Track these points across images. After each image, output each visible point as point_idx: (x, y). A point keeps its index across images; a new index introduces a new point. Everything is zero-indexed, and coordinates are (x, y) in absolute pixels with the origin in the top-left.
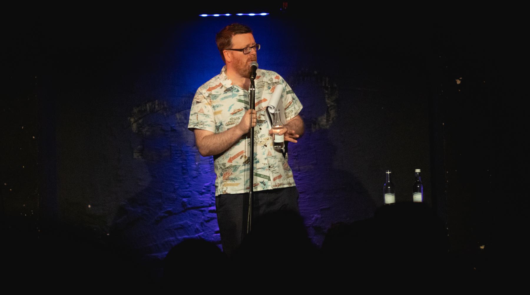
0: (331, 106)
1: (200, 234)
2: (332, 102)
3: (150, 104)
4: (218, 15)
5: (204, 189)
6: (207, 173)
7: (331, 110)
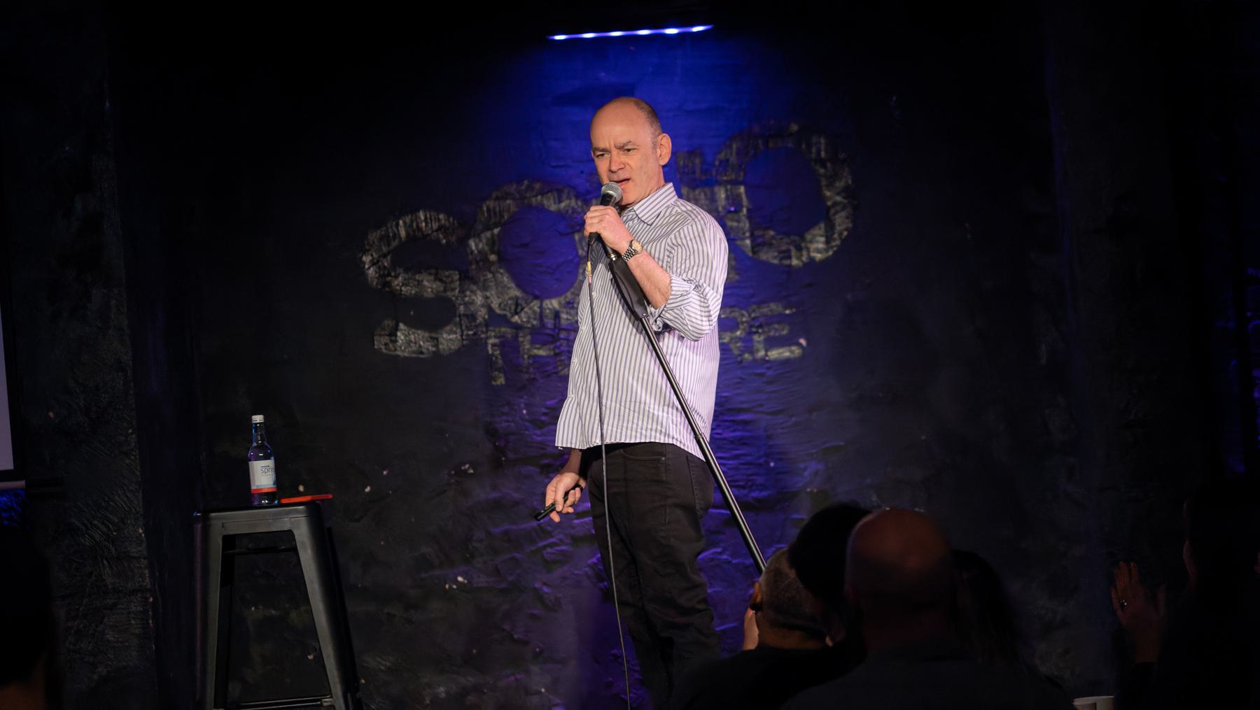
0: (835, 204)
1: (324, 496)
2: (838, 194)
3: (408, 220)
4: (558, 38)
5: (545, 414)
6: (549, 376)
7: (837, 212)
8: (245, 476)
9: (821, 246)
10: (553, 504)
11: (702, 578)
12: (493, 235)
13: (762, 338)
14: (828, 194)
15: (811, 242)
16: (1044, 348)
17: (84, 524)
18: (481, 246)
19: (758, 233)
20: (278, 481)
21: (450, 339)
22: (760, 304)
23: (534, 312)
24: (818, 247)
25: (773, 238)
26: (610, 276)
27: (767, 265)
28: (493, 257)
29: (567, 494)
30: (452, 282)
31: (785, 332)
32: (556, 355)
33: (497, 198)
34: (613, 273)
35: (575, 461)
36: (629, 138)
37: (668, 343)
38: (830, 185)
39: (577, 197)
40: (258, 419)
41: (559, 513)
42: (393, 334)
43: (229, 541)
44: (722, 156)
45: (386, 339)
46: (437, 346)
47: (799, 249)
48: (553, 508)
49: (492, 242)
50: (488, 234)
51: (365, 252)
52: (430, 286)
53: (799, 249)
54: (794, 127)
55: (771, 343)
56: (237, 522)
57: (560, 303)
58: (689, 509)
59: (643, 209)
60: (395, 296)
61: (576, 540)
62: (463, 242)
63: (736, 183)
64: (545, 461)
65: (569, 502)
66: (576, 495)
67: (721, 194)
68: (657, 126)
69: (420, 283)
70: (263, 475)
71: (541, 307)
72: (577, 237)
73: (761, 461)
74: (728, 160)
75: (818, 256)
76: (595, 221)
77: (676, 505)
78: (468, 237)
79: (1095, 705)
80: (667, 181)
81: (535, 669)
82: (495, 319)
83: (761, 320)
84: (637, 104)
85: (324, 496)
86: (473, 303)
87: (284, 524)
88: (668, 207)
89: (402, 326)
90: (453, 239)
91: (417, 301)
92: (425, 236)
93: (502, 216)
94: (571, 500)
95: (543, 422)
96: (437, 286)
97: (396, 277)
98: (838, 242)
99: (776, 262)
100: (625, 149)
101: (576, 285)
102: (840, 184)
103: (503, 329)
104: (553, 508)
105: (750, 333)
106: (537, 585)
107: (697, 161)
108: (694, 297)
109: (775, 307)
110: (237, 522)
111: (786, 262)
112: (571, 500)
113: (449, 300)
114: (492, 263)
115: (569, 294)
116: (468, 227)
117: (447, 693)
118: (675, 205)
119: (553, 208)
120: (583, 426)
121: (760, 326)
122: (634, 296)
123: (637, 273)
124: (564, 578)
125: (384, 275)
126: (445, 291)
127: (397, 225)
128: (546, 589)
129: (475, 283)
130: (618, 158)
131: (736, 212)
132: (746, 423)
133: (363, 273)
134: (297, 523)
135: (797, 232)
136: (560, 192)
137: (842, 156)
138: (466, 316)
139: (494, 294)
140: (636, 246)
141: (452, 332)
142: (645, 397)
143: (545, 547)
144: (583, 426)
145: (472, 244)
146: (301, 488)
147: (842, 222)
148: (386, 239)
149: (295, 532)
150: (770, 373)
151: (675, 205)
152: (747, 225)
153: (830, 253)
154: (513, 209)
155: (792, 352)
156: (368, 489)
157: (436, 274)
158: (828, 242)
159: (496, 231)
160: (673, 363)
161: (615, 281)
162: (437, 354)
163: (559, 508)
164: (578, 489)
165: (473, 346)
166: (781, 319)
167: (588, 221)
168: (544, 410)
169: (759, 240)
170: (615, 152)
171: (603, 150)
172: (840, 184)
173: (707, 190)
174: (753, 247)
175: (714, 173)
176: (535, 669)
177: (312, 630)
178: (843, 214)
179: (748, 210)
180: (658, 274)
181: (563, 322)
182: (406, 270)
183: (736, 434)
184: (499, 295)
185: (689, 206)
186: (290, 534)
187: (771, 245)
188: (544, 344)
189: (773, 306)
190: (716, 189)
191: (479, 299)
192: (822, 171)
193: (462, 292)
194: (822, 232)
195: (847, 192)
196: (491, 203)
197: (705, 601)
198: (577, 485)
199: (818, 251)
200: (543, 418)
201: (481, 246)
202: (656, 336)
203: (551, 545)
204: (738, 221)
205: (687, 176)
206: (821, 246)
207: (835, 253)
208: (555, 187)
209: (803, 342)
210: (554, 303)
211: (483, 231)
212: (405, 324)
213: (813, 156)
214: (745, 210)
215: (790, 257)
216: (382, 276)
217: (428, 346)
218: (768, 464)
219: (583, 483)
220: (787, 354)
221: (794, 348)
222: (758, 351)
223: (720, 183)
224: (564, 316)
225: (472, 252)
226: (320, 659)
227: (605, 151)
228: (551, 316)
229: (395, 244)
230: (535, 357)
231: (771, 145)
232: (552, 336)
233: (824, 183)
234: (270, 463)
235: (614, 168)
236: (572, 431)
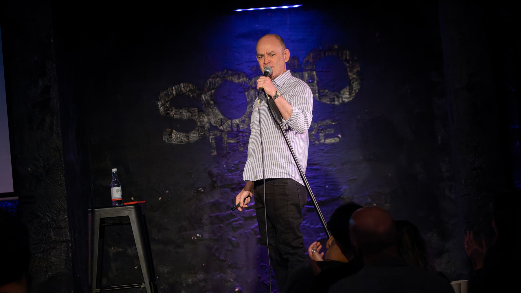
0: (353, 78)
1: (142, 202)
2: (354, 74)
5: (233, 167)
6: (235, 151)
7: (353, 83)
8: (109, 193)
9: (347, 96)
10: (239, 204)
11: (300, 234)
12: (211, 93)
13: (323, 134)
14: (350, 74)
15: (343, 94)
16: (439, 138)
17: (43, 215)
18: (207, 97)
19: (321, 91)
20: (123, 195)
21: (194, 136)
22: (322, 120)
23: (229, 125)
24: (346, 96)
25: (327, 93)
26: (267, 106)
27: (325, 104)
28: (212, 102)
29: (245, 199)
30: (195, 112)
31: (332, 132)
32: (238, 142)
33: (213, 78)
34: (268, 104)
35: (248, 186)
36: (272, 51)
37: (290, 135)
38: (351, 71)
39: (247, 76)
40: (115, 170)
42: (170, 134)
43: (103, 220)
45: (167, 137)
46: (188, 139)
47: (338, 97)
49: (211, 96)
50: (210, 93)
51: (159, 100)
52: (185, 114)
53: (338, 97)
54: (336, 47)
55: (327, 137)
56: (106, 212)
57: (239, 121)
58: (297, 206)
59: (278, 81)
60: (171, 119)
61: (246, 219)
62: (199, 95)
63: (312, 70)
64: (233, 186)
65: (245, 203)
67: (306, 75)
68: (284, 46)
69: (181, 113)
70: (116, 193)
71: (231, 123)
72: (246, 93)
73: (323, 185)
74: (308, 61)
75: (346, 100)
76: (262, 83)
78: (201, 94)
79: (460, 284)
80: (287, 69)
81: (229, 271)
82: (213, 128)
83: (323, 127)
84: (276, 36)
85: (142, 202)
86: (203, 121)
87: (126, 213)
89: (174, 131)
90: (195, 95)
91: (180, 120)
92: (183, 94)
93: (215, 85)
94: (246, 202)
96: (189, 114)
97: (172, 111)
98: (354, 94)
99: (329, 103)
100: (271, 54)
101: (316, 88)
102: (355, 70)
103: (216, 132)
105: (318, 133)
106: (230, 237)
107: (296, 61)
108: (302, 116)
109: (328, 122)
110: (106, 212)
111: (333, 103)
112: (246, 202)
113: (193, 120)
114: (211, 105)
115: (243, 117)
116: (202, 90)
117: (192, 282)
118: (291, 79)
119: (236, 81)
120: (254, 172)
121: (322, 130)
123: (278, 105)
124: (241, 235)
125: (167, 110)
126: (192, 116)
127: (172, 89)
129: (204, 113)
130: (268, 58)
131: (312, 82)
132: (317, 170)
133: (158, 110)
134: (131, 213)
135: (337, 90)
136: (239, 75)
137: (356, 58)
138: (201, 127)
139: (213, 117)
140: (279, 94)
141: (195, 133)
142: (279, 158)
143: (233, 222)
144: (254, 172)
145: (203, 96)
146: (132, 198)
147: (356, 86)
148: (167, 95)
149: (130, 217)
150: (326, 149)
151: (291, 79)
153: (351, 99)
154: (220, 82)
155: (335, 140)
156: (160, 199)
157: (188, 110)
158: (350, 94)
159: (213, 91)
160: (293, 145)
161: (269, 107)
162: (188, 143)
163: (242, 205)
165: (204, 139)
166: (331, 126)
167: (259, 83)
168: (233, 165)
169: (322, 94)
170: (266, 56)
171: (262, 55)
172: (355, 70)
173: (300, 73)
174: (319, 97)
176: (229, 271)
177: (137, 257)
178: (357, 83)
179: (317, 81)
180: (287, 105)
181: (241, 129)
182: (176, 108)
183: (312, 174)
184: (215, 117)
185: (297, 79)
186: (127, 217)
187: (327, 96)
189: (327, 121)
190: (304, 73)
191: (206, 120)
192: (348, 65)
193: (199, 117)
194: (348, 90)
195: (358, 73)
196: (211, 80)
197: (302, 243)
198: (249, 196)
199: (346, 98)
200: (233, 169)
201: (207, 97)
202: (282, 133)
203: (236, 221)
204: (313, 86)
205: (295, 67)
206: (347, 96)
207: (353, 99)
208: (238, 73)
209: (340, 136)
210: (237, 121)
211: (208, 91)
212: (176, 130)
213: (344, 59)
214: (316, 82)
215: (334, 101)
216: (165, 111)
217: (185, 139)
218: (325, 186)
220: (333, 141)
221: (336, 138)
222: (321, 140)
223: (306, 70)
224: (241, 126)
225: (203, 100)
226: (140, 269)
227: (263, 56)
228: (235, 126)
229: (171, 97)
231: (327, 54)
232: (236, 134)
233: (348, 69)
234: (119, 188)
235: (266, 62)
236: (251, 173)
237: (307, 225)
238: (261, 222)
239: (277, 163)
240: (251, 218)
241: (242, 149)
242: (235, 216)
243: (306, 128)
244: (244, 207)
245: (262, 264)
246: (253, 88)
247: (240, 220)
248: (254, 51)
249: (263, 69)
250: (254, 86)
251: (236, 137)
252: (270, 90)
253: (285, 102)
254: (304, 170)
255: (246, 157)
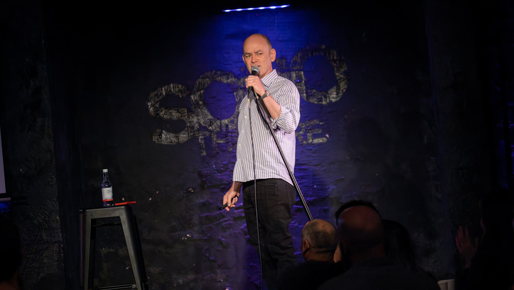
5: (222, 167)
6: (224, 151)
11: (289, 234)
23: (218, 125)
29: (232, 199)
32: (227, 143)
36: (258, 51)
37: (279, 135)
39: (235, 77)
41: (229, 207)
44: (294, 59)
48: (226, 205)
57: (228, 121)
61: (235, 219)
63: (300, 70)
64: (222, 187)
66: (236, 199)
67: (294, 75)
71: (220, 123)
72: (235, 93)
74: (296, 61)
76: (252, 81)
77: (281, 204)
80: (273, 68)
81: (219, 271)
88: (275, 79)
94: (234, 202)
95: (221, 170)
104: (226, 205)
107: (284, 61)
112: (234, 202)
115: (232, 118)
119: (225, 81)
120: (244, 172)
122: (265, 113)
128: (223, 239)
130: (255, 57)
136: (228, 75)
142: (269, 158)
143: (222, 222)
144: (244, 172)
151: (278, 79)
152: (305, 88)
163: (229, 205)
164: (236, 197)
167: (249, 82)
168: (222, 166)
170: (254, 54)
171: (249, 54)
173: (288, 73)
175: (291, 66)
176: (219, 271)
179: (305, 81)
185: (284, 79)
188: (222, 138)
190: (292, 73)
197: (291, 243)
198: (236, 196)
203: (225, 221)
204: (301, 86)
205: (282, 67)
208: (226, 73)
210: (226, 121)
214: (303, 82)
219: (238, 195)
223: (293, 70)
224: (230, 126)
227: (250, 55)
230: (219, 143)
232: (225, 135)
235: (253, 61)
236: (241, 173)
237: (296, 225)
238: (250, 222)
239: (266, 163)
240: (240, 218)
241: (231, 149)
242: (224, 217)
243: (295, 128)
244: (231, 206)
245: (251, 264)
246: (241, 88)
247: (229, 220)
248: (241, 51)
249: (250, 69)
250: (242, 86)
251: (225, 137)
252: (259, 90)
253: (273, 101)
254: (292, 170)
255: (235, 158)
